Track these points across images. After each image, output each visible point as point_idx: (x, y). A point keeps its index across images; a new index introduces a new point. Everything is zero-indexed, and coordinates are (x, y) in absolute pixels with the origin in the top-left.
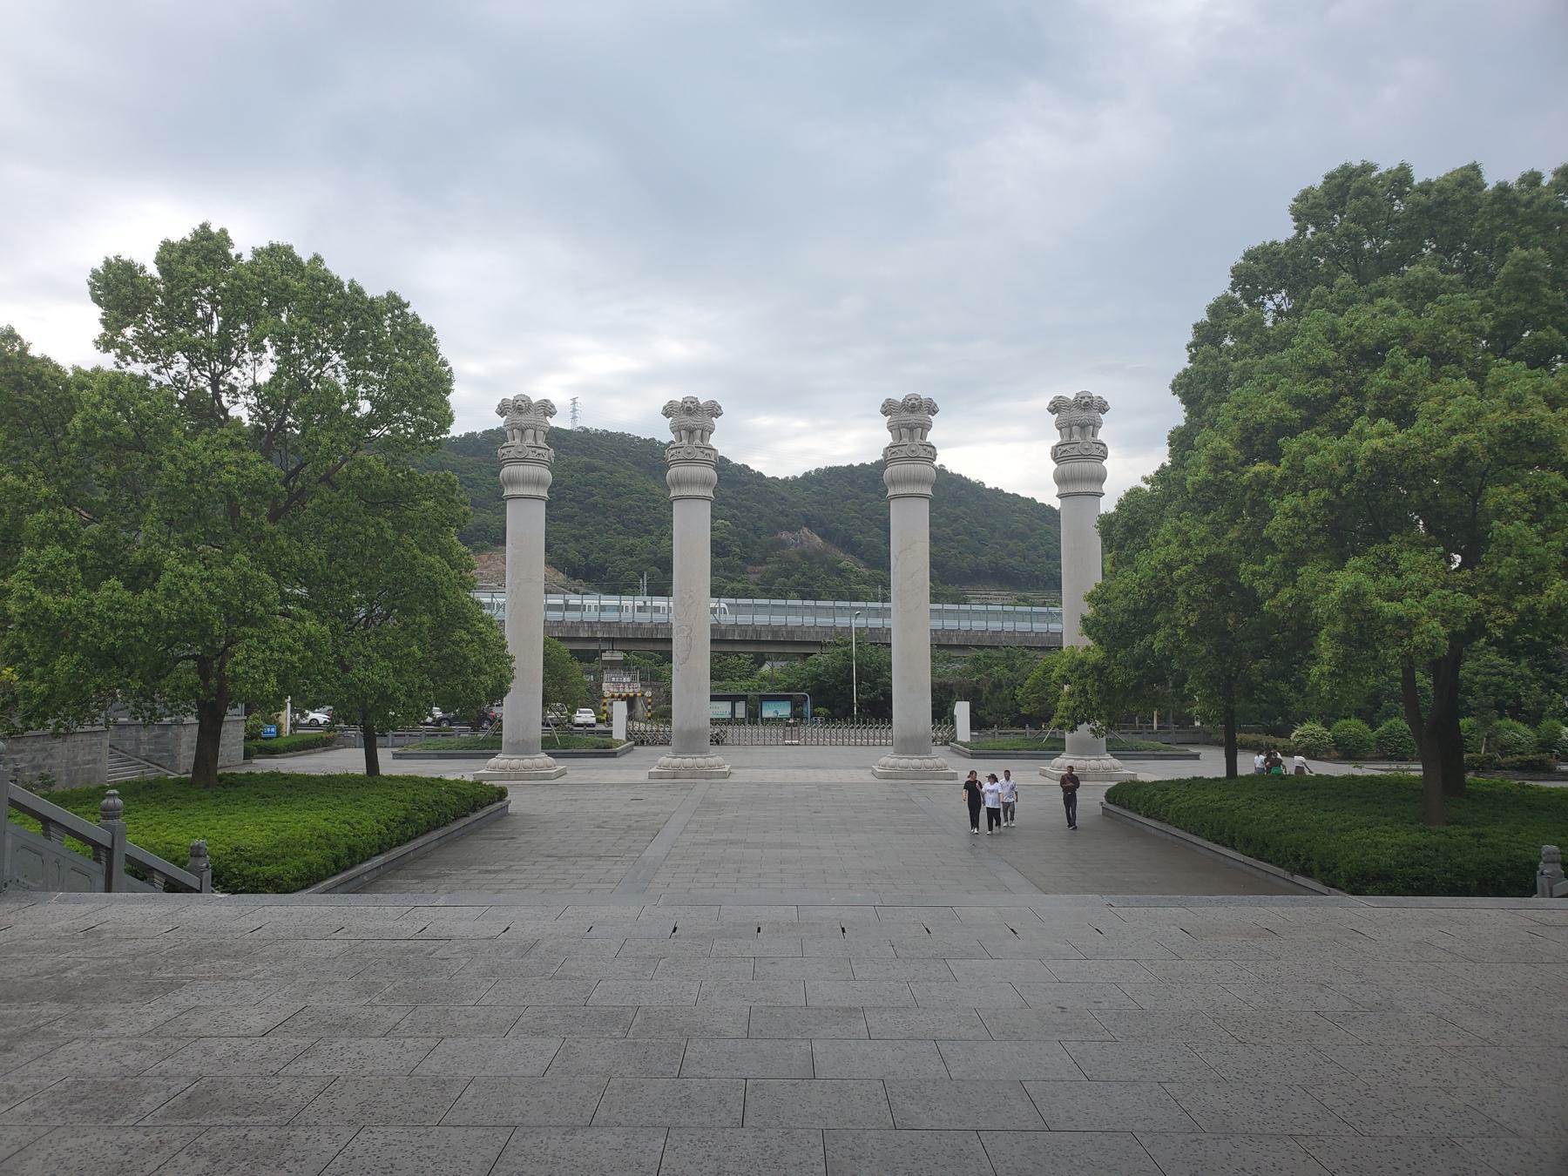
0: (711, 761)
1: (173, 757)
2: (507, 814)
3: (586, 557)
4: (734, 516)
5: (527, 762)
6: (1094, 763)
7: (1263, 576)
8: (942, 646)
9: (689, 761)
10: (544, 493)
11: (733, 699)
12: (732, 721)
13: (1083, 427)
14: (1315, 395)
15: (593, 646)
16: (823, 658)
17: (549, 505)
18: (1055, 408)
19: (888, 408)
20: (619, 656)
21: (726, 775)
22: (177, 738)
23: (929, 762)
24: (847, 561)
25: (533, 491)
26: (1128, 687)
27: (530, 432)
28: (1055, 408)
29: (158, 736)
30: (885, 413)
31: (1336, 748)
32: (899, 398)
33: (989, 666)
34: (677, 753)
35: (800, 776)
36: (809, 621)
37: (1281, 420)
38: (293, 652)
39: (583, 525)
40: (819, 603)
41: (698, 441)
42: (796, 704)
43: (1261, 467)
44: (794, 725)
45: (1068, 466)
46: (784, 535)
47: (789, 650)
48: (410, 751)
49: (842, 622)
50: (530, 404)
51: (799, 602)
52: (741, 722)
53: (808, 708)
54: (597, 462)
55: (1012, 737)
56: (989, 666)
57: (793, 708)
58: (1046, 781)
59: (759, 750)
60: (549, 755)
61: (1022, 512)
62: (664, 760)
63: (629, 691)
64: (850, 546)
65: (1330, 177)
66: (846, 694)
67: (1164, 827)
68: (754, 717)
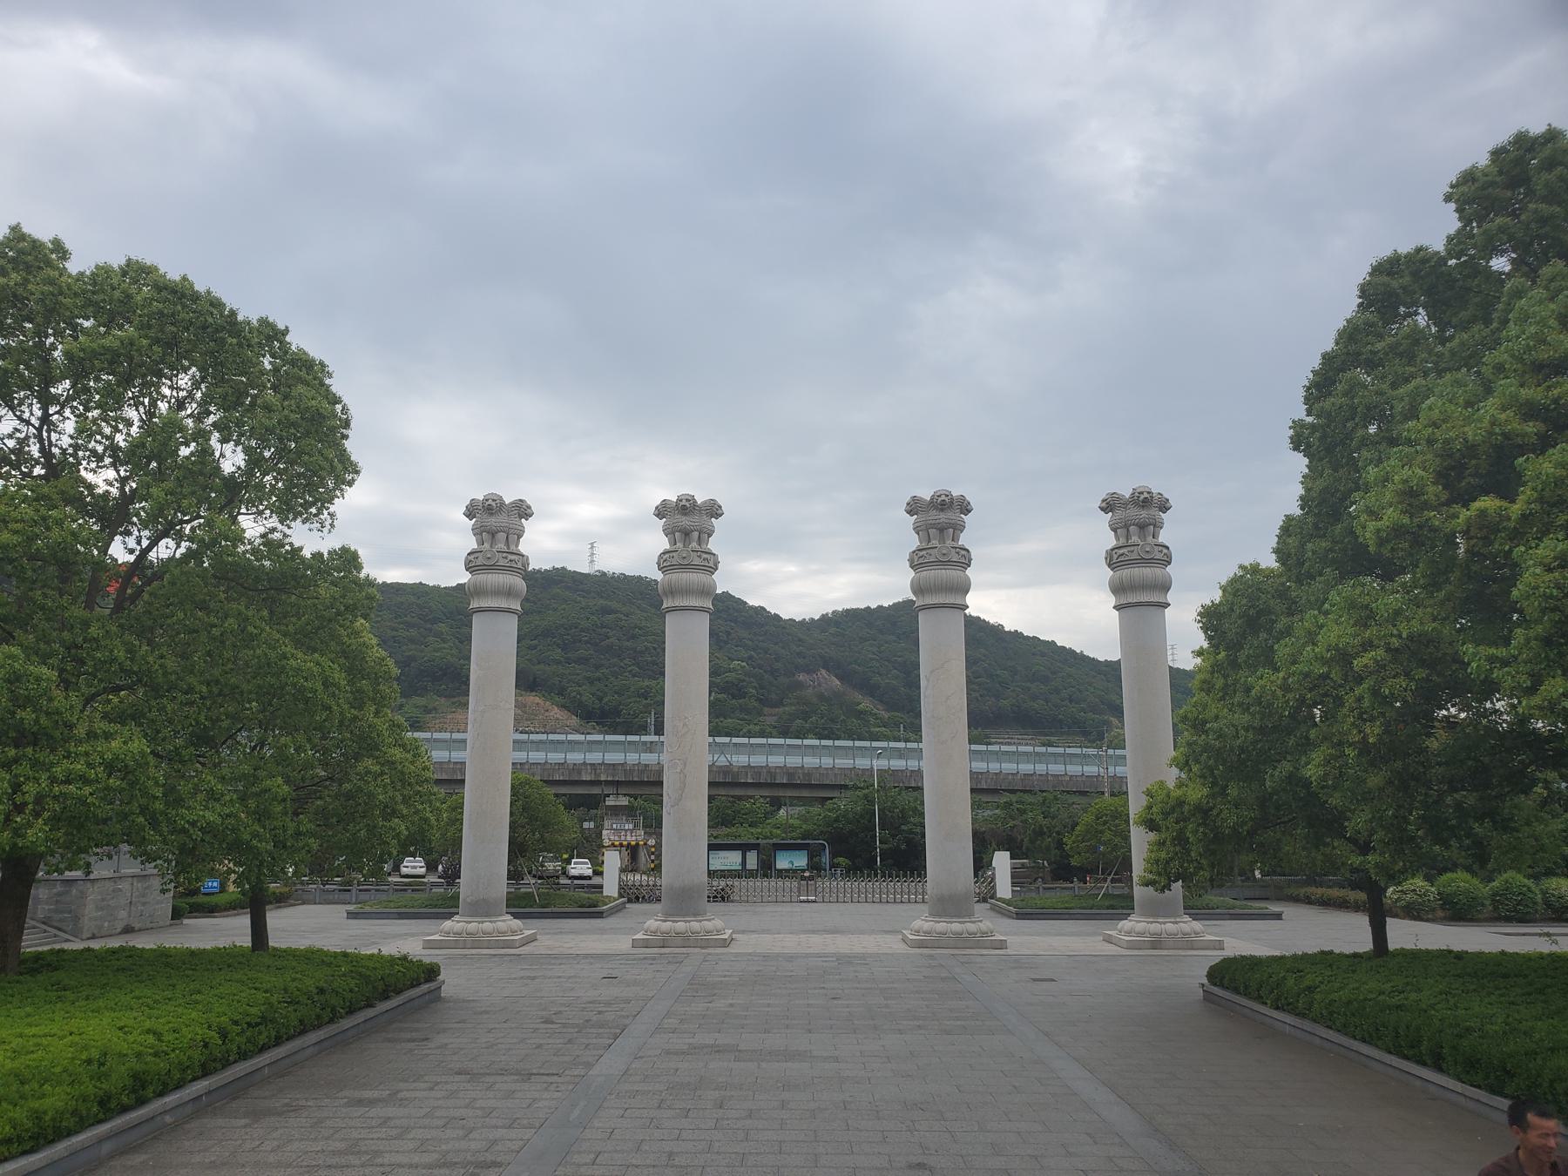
0: (708, 925)
1: (76, 919)
2: (439, 999)
3: (600, 699)
4: (751, 658)
5: (487, 926)
6: (1170, 927)
7: (1505, 663)
8: (981, 791)
9: (681, 926)
10: (516, 605)
11: (744, 848)
12: (743, 873)
13: (1142, 527)
14: (1556, 401)
15: (596, 790)
16: (843, 803)
17: (523, 617)
18: (1109, 505)
19: (914, 507)
20: (624, 801)
21: (725, 943)
22: (83, 895)
23: (972, 927)
24: (866, 704)
25: (503, 604)
26: (1239, 832)
27: (502, 536)
28: (1109, 505)
29: (59, 894)
30: (910, 512)
31: (1442, 907)
32: (926, 494)
33: (1022, 812)
34: (668, 915)
35: (817, 943)
36: (827, 762)
37: (1506, 436)
38: (85, 780)
39: (597, 667)
40: (837, 743)
41: (694, 545)
42: (813, 854)
43: (1487, 503)
44: (811, 878)
45: (1126, 573)
46: (802, 677)
47: (805, 793)
48: (368, 909)
49: (862, 763)
50: (502, 503)
51: (816, 742)
52: (751, 874)
53: (826, 859)
54: (614, 605)
55: (1060, 894)
56: (1022, 812)
57: (810, 858)
58: (1111, 949)
59: (770, 908)
60: (516, 916)
61: (1043, 655)
62: (652, 924)
63: (631, 839)
64: (870, 690)
65: (1497, 154)
66: (872, 844)
67: (1307, 1025)
68: (767, 868)
